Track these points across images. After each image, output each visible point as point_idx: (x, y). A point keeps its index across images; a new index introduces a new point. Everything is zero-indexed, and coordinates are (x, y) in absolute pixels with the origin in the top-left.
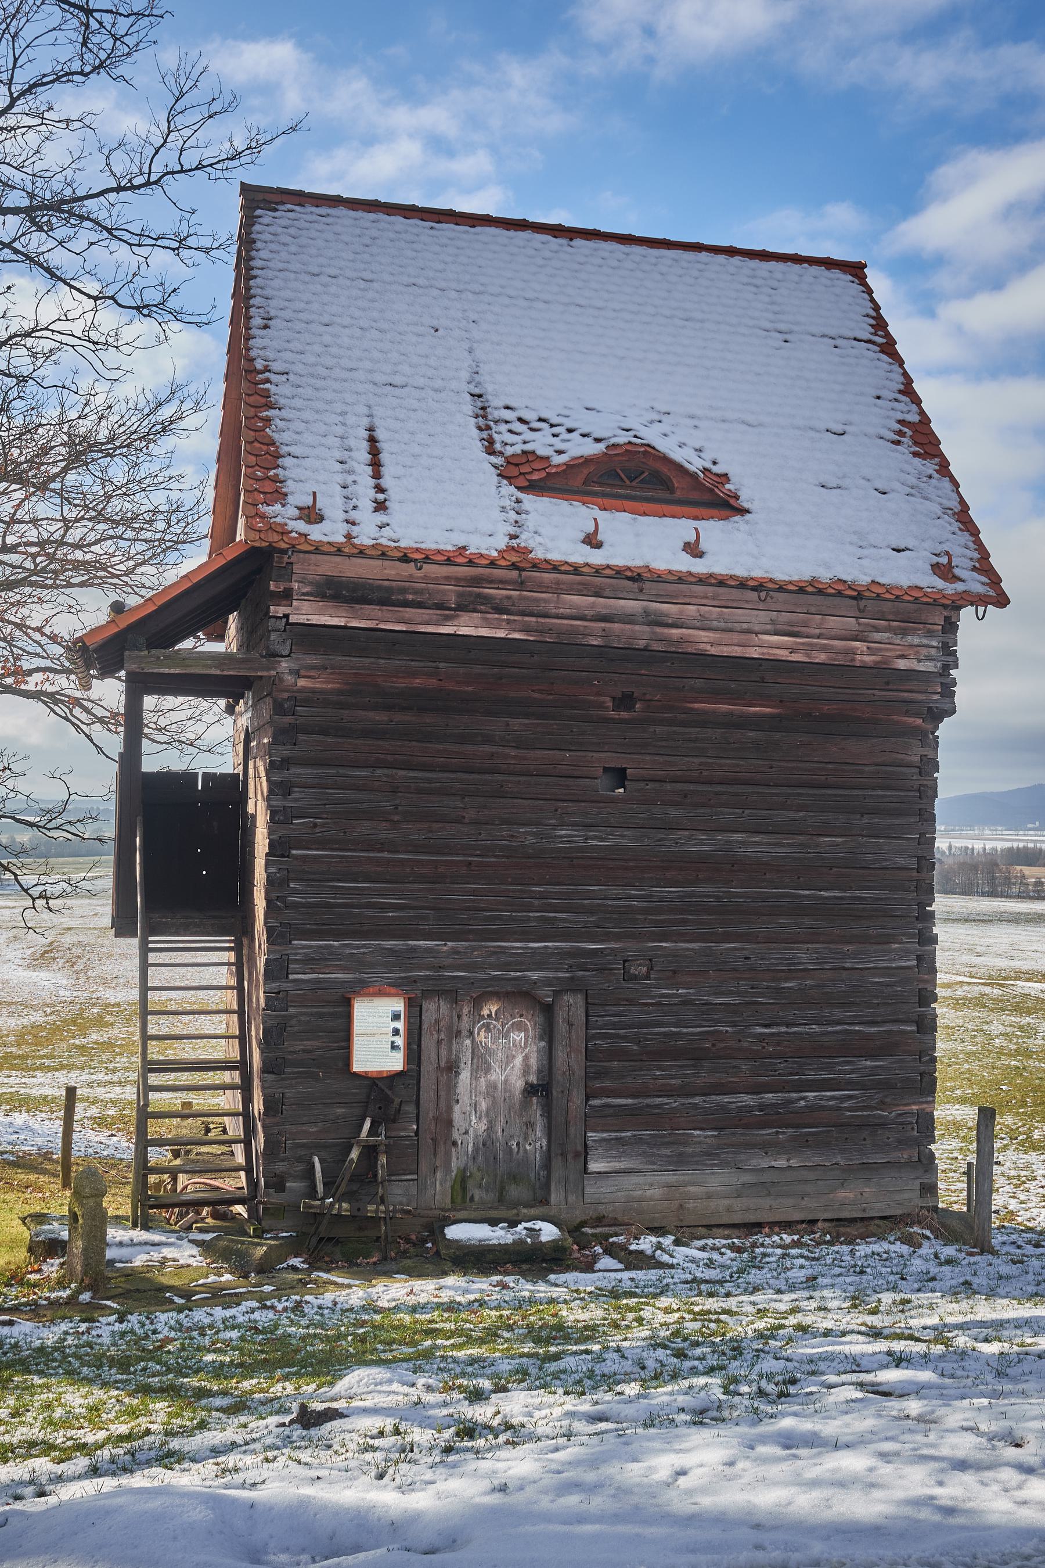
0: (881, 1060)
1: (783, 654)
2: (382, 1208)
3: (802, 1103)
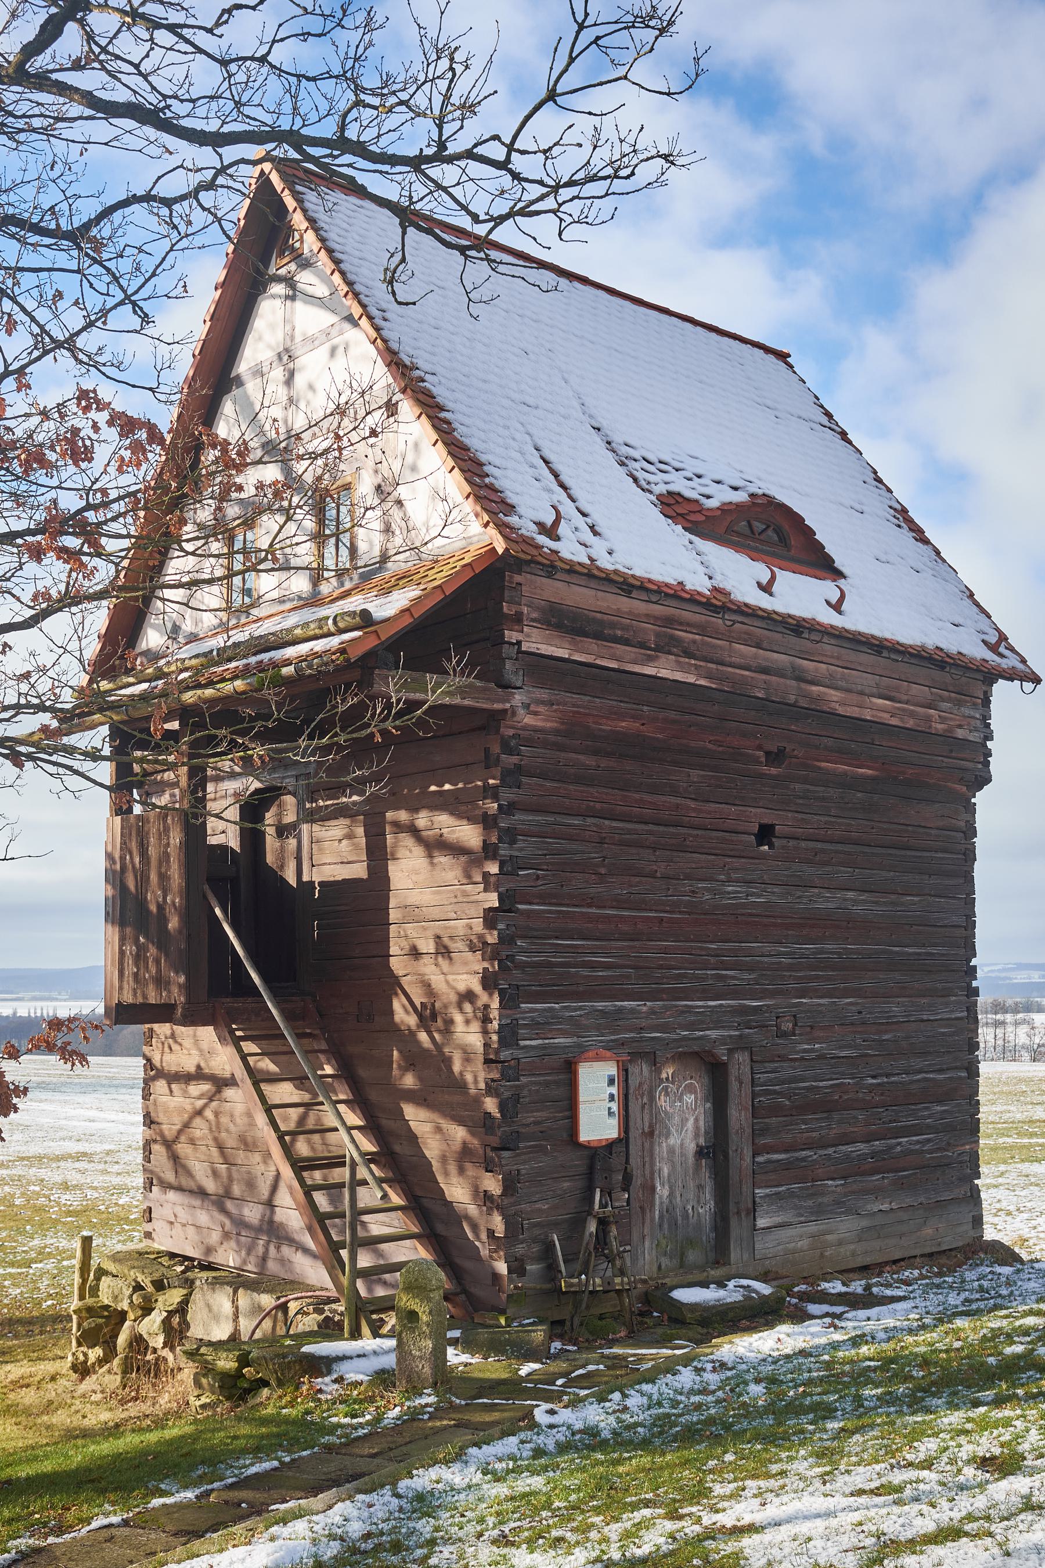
0: (946, 1105)
1: (885, 717)
2: (626, 1279)
3: (899, 1148)
